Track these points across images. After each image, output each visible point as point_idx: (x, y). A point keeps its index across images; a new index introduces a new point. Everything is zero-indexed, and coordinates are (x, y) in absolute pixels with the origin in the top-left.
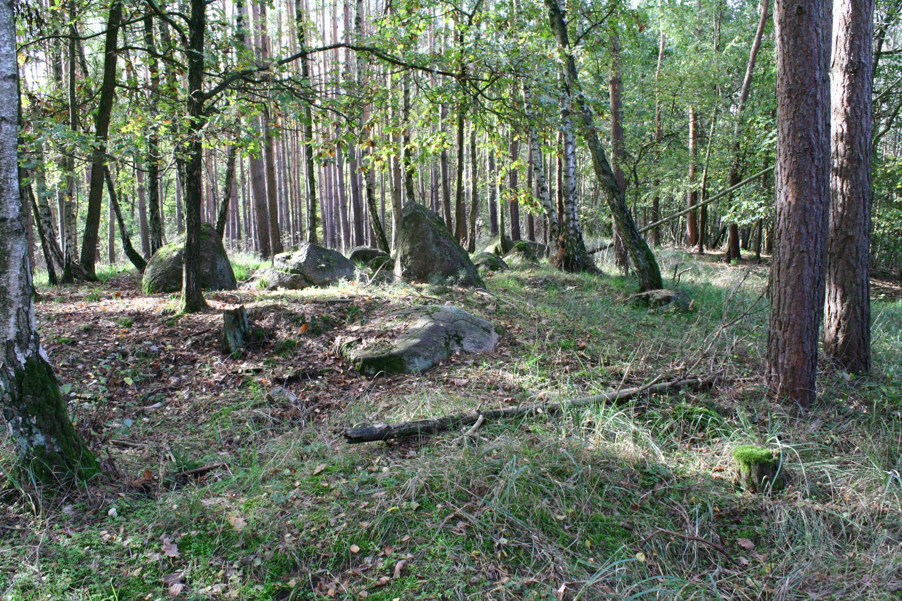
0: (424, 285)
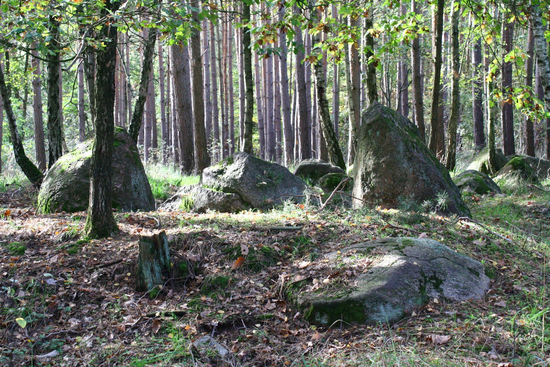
0: (392, 211)
